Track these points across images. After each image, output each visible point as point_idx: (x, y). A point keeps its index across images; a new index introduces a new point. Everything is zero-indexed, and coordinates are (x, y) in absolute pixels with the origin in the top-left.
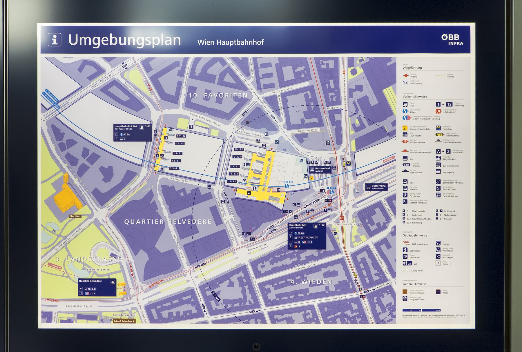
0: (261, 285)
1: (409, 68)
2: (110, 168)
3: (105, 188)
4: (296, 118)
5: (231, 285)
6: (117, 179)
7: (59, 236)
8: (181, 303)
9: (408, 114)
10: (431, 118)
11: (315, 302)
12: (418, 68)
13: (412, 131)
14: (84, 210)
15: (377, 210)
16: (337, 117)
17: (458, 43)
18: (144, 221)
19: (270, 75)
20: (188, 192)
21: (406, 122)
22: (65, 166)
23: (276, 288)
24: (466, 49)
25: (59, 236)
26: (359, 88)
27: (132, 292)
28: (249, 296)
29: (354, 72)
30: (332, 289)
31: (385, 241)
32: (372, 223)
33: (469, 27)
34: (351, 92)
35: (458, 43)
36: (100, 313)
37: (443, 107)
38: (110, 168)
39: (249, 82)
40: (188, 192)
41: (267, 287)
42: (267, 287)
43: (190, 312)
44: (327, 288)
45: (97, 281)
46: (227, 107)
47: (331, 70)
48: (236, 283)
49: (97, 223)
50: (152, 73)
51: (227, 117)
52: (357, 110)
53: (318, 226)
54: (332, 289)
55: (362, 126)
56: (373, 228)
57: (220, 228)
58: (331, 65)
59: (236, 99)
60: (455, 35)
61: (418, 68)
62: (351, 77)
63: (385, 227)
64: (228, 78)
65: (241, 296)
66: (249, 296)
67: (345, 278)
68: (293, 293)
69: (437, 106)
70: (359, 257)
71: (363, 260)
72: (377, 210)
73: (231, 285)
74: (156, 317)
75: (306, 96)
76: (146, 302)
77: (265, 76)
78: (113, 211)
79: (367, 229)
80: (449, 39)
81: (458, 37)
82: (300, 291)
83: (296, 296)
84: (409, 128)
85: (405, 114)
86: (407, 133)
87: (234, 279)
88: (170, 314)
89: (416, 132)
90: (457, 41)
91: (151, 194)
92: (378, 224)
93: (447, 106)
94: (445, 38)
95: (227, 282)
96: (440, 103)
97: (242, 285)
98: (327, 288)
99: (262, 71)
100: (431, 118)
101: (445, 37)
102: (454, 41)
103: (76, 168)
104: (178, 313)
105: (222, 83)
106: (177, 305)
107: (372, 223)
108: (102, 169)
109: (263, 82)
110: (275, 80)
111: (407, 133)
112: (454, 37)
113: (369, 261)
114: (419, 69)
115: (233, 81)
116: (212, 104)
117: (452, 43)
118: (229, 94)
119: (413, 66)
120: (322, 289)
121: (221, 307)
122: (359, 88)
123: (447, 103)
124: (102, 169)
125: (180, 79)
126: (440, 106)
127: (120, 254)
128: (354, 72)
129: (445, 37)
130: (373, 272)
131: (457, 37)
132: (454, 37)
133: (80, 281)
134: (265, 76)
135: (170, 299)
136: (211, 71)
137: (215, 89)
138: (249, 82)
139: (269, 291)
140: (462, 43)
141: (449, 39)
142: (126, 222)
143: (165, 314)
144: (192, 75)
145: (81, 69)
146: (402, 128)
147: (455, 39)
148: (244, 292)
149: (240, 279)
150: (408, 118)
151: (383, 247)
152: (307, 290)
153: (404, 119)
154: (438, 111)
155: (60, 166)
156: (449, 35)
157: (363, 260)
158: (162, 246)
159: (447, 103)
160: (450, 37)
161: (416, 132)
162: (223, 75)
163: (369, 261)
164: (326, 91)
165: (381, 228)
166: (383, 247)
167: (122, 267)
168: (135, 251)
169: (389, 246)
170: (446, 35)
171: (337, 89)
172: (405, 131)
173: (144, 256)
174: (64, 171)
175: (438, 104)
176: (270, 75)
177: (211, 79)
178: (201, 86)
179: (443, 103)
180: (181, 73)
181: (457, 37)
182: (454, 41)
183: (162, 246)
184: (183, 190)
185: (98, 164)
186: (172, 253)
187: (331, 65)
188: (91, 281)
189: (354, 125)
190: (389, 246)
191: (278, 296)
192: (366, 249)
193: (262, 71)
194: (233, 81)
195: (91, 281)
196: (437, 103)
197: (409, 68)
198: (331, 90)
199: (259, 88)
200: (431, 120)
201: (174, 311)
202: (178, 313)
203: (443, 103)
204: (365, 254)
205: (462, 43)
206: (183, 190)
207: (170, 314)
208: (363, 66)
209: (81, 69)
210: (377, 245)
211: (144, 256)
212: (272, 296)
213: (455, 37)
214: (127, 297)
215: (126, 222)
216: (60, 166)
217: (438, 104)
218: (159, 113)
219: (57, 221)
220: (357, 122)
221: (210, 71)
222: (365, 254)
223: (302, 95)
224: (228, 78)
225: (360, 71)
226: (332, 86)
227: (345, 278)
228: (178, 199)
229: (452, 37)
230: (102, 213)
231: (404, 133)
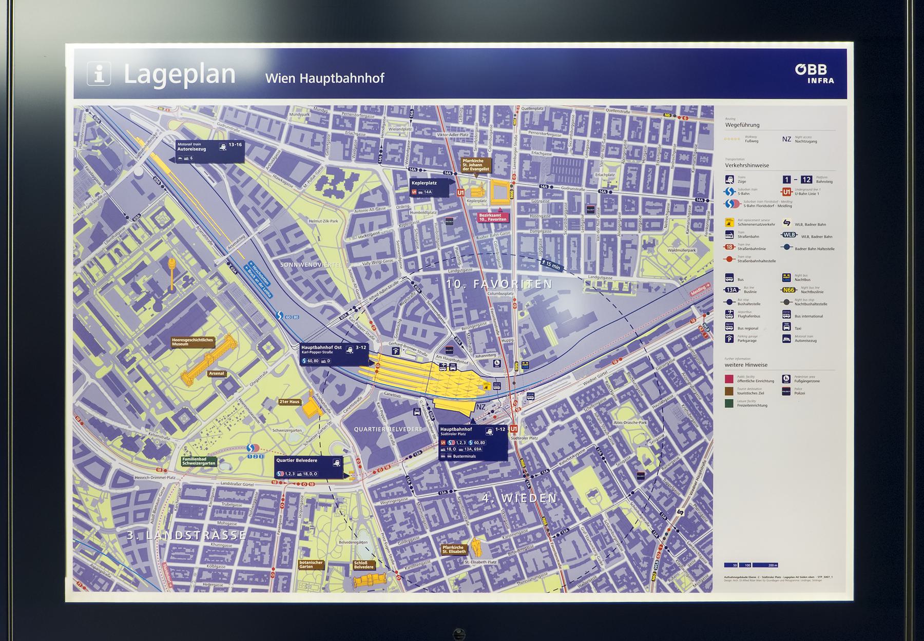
0: (454, 472)
1: (736, 126)
2: (344, 385)
3: (340, 400)
4: (480, 347)
5: (432, 472)
6: (348, 394)
7: (306, 436)
8: (395, 486)
9: (735, 197)
10: (776, 204)
11: (493, 486)
12: (753, 125)
13: (743, 228)
14: (325, 417)
15: (539, 417)
16: (510, 348)
17: (825, 80)
18: (370, 429)
19: (461, 316)
20: (401, 403)
21: (731, 212)
22: (310, 384)
23: (465, 474)
24: (838, 92)
25: (306, 436)
26: (526, 326)
27: (359, 478)
28: (445, 481)
29: (522, 314)
30: (506, 475)
31: (544, 440)
32: (536, 427)
33: (844, 52)
34: (520, 329)
35: (825, 80)
36: (336, 493)
37: (796, 185)
38: (344, 385)
39: (446, 321)
40: (401, 403)
41: (459, 473)
42: (459, 473)
43: (402, 492)
44: (502, 475)
45: (310, 461)
46: (429, 339)
47: (506, 313)
48: (436, 471)
49: (334, 427)
50: (375, 315)
51: (429, 347)
52: (524, 343)
53: (494, 431)
54: (506, 475)
55: (528, 355)
56: (536, 430)
57: (424, 430)
58: (506, 309)
59: (436, 334)
60: (820, 66)
61: (753, 125)
62: (520, 318)
63: (545, 430)
64: (430, 319)
65: (439, 481)
66: (445, 481)
67: (516, 467)
68: (477, 478)
69: (785, 182)
70: (526, 452)
71: (529, 453)
72: (539, 417)
73: (432, 472)
74: (376, 496)
75: (487, 332)
76: (369, 485)
77: (457, 317)
78: (345, 418)
79: (532, 431)
80: (810, 73)
81: (824, 69)
82: (483, 477)
83: (480, 481)
84: (737, 222)
85: (730, 198)
86: (732, 232)
87: (434, 468)
88: (387, 494)
89: (748, 231)
90: (823, 77)
91: (373, 405)
92: (540, 427)
93: (802, 182)
94: (801, 70)
95: (429, 470)
96: (789, 177)
97: (440, 472)
98: (502, 475)
99: (455, 314)
100: (776, 204)
101: (801, 69)
102: (817, 76)
103: (318, 386)
104: (393, 493)
105: (425, 322)
106: (392, 487)
107: (536, 427)
108: (337, 386)
109: (456, 321)
110: (464, 320)
111: (732, 232)
112: (817, 69)
113: (533, 455)
114: (755, 128)
115: (434, 321)
116: (418, 338)
117: (814, 81)
118: (431, 330)
119: (744, 122)
120: (498, 475)
121: (425, 488)
122: (526, 326)
123: (802, 177)
124: (337, 386)
125: (394, 319)
126: (789, 182)
127: (351, 449)
128: (522, 314)
129: (801, 69)
130: (536, 462)
131: (823, 69)
132: (817, 69)
133: (279, 461)
134: (457, 317)
135: (387, 483)
136: (418, 313)
137: (421, 326)
138: (446, 321)
139: (459, 476)
140: (831, 81)
141: (810, 73)
142: (357, 429)
143: (383, 494)
144: (404, 316)
145: (322, 312)
146: (724, 223)
147: (820, 73)
148: (441, 477)
149: (438, 468)
150: (735, 204)
151: (543, 444)
152: (487, 476)
153: (728, 206)
154: (786, 192)
155: (307, 384)
156: (809, 66)
157: (529, 453)
158: (381, 444)
159: (802, 177)
160: (811, 69)
161: (748, 231)
162: (426, 316)
163: (533, 455)
164: (502, 328)
165: (542, 430)
166: (543, 444)
167: (352, 459)
168: (362, 447)
169: (547, 444)
170: (803, 66)
171: (510, 328)
172: (729, 229)
173: (368, 451)
174: (310, 388)
175: (787, 179)
176: (461, 316)
177: (418, 319)
178: (411, 325)
179: (796, 176)
180: (396, 315)
181: (823, 69)
182: (817, 76)
183: (381, 444)
184: (397, 402)
185: (335, 382)
186: (388, 449)
187: (506, 309)
188: (297, 460)
189: (522, 354)
190: (547, 444)
191: (466, 480)
192: (531, 445)
193: (455, 314)
194: (434, 321)
195: (297, 460)
196: (784, 177)
197: (736, 126)
198: (506, 328)
199: (453, 326)
200: (776, 207)
201: (390, 492)
202: (393, 493)
203: (796, 176)
204: (530, 450)
205: (831, 81)
206: (397, 402)
207: (387, 494)
208: (529, 310)
209: (322, 312)
210: (539, 443)
211: (368, 451)
212: (461, 481)
213: (820, 69)
214: (356, 481)
215: (357, 429)
216: (307, 384)
217: (787, 179)
218: (379, 345)
219: (303, 423)
220: (525, 351)
221: (416, 314)
222: (530, 450)
223: (484, 331)
224: (430, 319)
225: (527, 313)
226: (507, 325)
227: (516, 467)
228: (392, 409)
229: (814, 69)
230: (337, 419)
231: (728, 232)
